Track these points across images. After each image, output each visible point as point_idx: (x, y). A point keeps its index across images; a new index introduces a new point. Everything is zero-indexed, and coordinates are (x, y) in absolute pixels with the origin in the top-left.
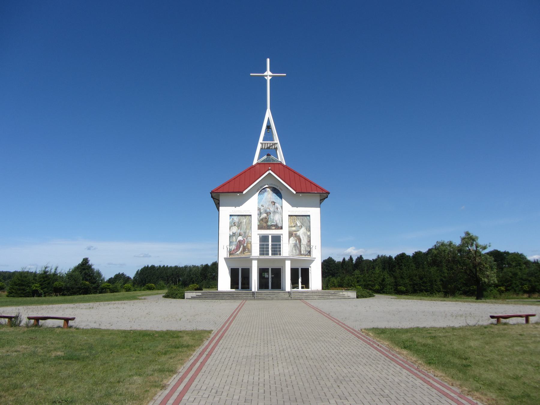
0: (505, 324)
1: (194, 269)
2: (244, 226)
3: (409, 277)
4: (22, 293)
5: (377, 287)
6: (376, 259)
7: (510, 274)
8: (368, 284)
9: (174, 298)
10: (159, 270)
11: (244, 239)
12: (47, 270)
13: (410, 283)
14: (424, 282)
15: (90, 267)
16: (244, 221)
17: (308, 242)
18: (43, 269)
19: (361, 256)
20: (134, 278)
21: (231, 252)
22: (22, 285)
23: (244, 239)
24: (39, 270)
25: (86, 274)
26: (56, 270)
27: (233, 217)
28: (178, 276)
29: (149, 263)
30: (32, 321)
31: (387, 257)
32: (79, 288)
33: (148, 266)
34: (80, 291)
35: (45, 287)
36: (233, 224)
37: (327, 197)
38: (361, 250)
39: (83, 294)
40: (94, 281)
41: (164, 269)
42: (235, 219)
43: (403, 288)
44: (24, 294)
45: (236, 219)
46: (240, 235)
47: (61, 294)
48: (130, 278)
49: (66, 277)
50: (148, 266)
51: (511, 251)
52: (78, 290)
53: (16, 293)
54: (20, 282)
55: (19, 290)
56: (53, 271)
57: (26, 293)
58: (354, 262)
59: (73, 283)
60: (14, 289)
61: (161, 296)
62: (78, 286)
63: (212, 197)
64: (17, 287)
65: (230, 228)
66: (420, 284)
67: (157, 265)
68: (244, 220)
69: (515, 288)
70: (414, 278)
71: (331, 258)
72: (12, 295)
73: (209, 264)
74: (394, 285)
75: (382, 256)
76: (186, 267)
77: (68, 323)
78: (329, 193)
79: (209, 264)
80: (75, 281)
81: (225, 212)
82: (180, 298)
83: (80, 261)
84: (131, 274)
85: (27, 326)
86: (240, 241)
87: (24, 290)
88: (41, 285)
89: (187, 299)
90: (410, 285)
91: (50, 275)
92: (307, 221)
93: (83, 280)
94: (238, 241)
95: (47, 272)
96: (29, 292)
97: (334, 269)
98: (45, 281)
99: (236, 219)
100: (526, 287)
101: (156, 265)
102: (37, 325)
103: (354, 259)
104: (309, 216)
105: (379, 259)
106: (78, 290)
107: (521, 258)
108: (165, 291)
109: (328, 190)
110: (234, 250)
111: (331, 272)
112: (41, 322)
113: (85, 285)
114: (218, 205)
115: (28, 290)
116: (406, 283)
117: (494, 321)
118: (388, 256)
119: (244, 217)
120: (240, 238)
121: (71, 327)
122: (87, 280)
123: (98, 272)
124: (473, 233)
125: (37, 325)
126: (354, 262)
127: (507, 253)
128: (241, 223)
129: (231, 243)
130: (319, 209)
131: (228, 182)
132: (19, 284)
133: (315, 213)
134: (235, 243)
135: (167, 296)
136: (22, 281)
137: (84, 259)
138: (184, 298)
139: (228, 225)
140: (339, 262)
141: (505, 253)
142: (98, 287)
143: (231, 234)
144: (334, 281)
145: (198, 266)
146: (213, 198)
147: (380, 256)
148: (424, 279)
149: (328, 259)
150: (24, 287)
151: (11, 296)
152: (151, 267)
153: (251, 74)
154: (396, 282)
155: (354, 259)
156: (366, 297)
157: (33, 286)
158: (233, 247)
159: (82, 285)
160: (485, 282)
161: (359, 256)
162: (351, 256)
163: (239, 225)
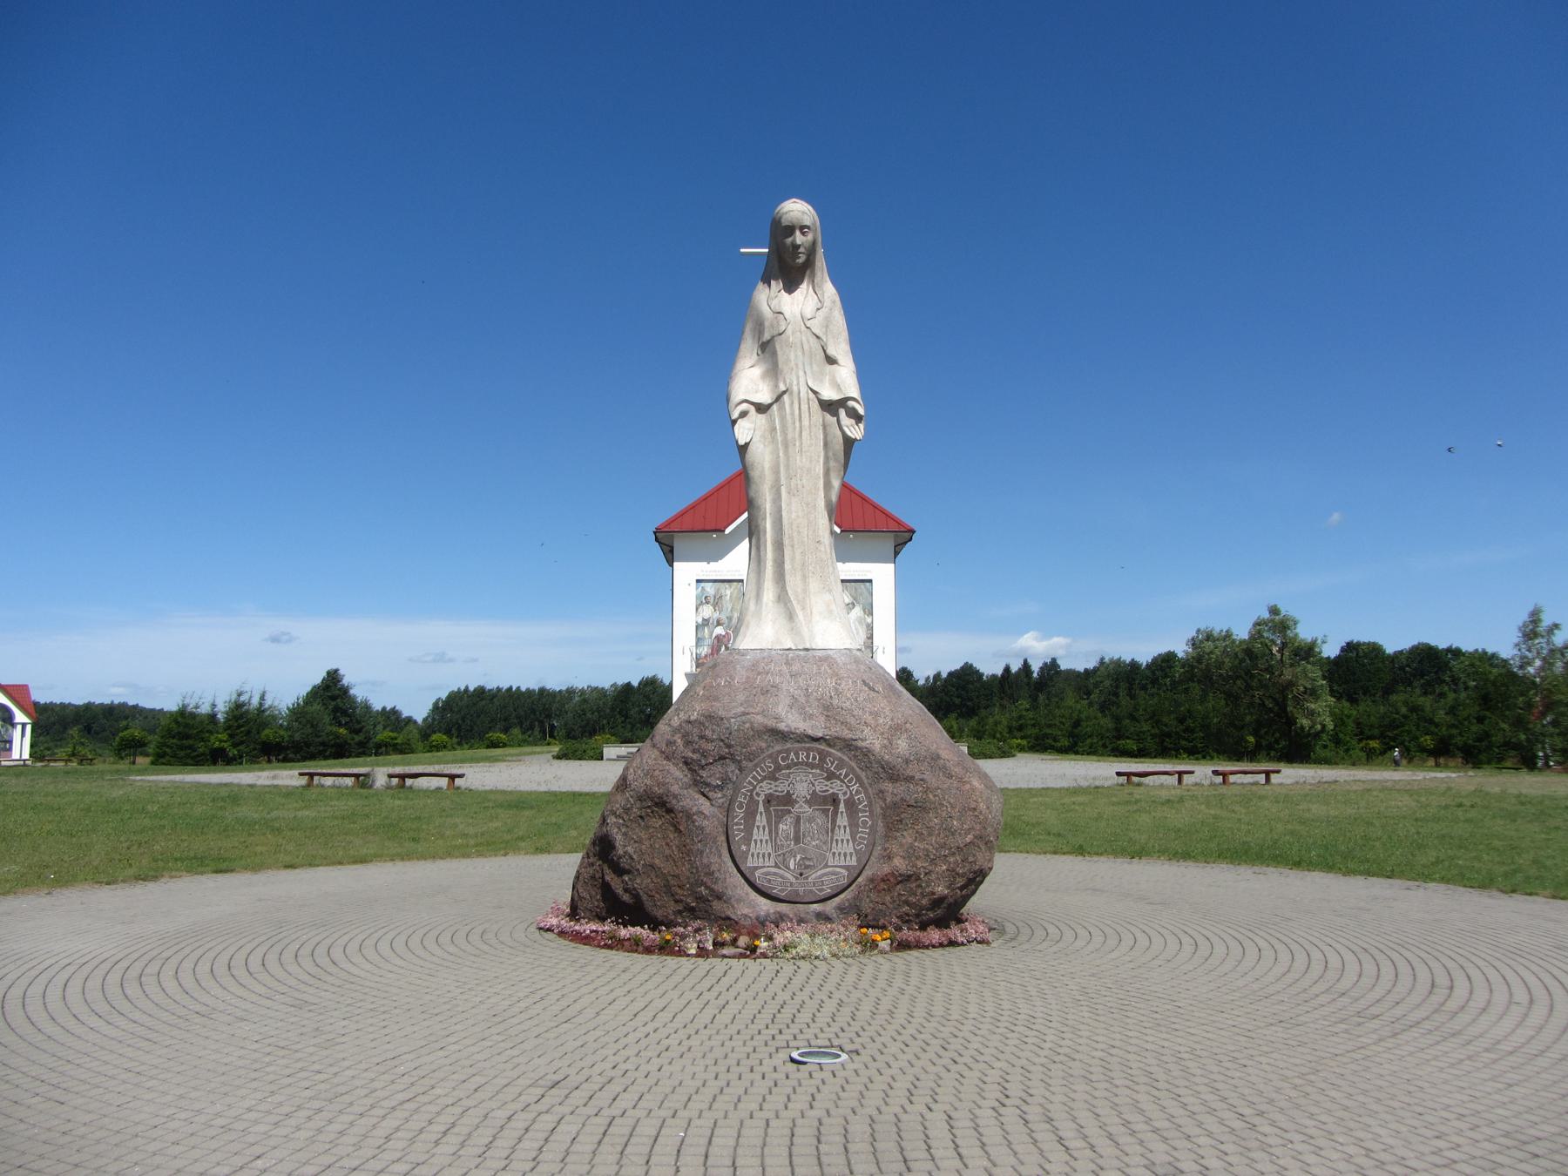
0: (1139, 785)
1: (595, 695)
2: (727, 603)
3: (1151, 718)
4: (187, 756)
5: (1065, 742)
6: (1096, 670)
7: (1404, 710)
8: (1046, 736)
9: (580, 759)
10: (495, 700)
11: (727, 633)
12: (242, 699)
13: (1153, 731)
14: (1187, 730)
15: (345, 691)
16: (728, 592)
17: (868, 638)
18: (234, 697)
19: (1054, 660)
20: (425, 720)
21: (701, 661)
22: (188, 737)
23: (727, 633)
24: (170, 704)
25: (336, 709)
26: (262, 698)
27: (703, 584)
28: (549, 716)
29: (471, 679)
30: (395, 781)
31: (1124, 662)
32: (323, 744)
33: (467, 687)
34: (325, 751)
35: (242, 743)
36: (702, 601)
37: (911, 539)
38: (1056, 640)
39: (334, 758)
40: (358, 727)
41: (512, 698)
42: (708, 589)
43: (1131, 745)
44: (192, 758)
45: (710, 589)
46: (719, 623)
47: (280, 757)
48: (415, 722)
49: (290, 716)
50: (467, 687)
51: (1467, 646)
52: (321, 748)
53: (174, 756)
54: (181, 729)
55: (182, 748)
56: (255, 701)
57: (198, 756)
58: (1035, 675)
59: (310, 731)
60: (168, 746)
61: (549, 756)
62: (320, 739)
63: (657, 540)
64: (175, 741)
65: (697, 609)
66: (1177, 733)
67: (491, 685)
68: (728, 591)
69: (1407, 743)
70: (1165, 719)
71: (971, 665)
72: (164, 761)
73: (635, 683)
74: (1113, 737)
75: (1112, 661)
76: (570, 692)
77: (454, 781)
78: (914, 532)
79: (635, 683)
80: (312, 726)
81: (687, 573)
82: (592, 758)
83: (317, 678)
84: (418, 709)
85: (389, 787)
86: (718, 637)
87: (190, 747)
88: (231, 736)
89: (608, 760)
90: (1153, 736)
91: (247, 711)
92: (866, 593)
93: (331, 725)
94: (714, 636)
95: (243, 704)
96: (203, 754)
97: (978, 697)
98: (239, 727)
99: (710, 589)
100: (1427, 741)
101: (488, 687)
102: (402, 786)
103: (1036, 667)
104: (870, 581)
105: (1102, 669)
106: (321, 748)
107: (1491, 665)
108: (556, 749)
109: (913, 525)
110: (706, 656)
111: (969, 703)
112: (409, 782)
113: (337, 736)
114: (671, 563)
115: (201, 748)
116: (1143, 733)
117: (1123, 779)
118: (1128, 660)
119: (727, 585)
120: (719, 630)
121: (458, 788)
122: (340, 725)
123: (366, 704)
124: (1286, 609)
125: (402, 786)
126: (1035, 675)
127: (1456, 653)
128: (721, 597)
129: (699, 641)
130: (892, 566)
131: (693, 507)
132: (179, 733)
133: (882, 575)
134: (708, 642)
135: (558, 757)
136: (187, 725)
137: (328, 673)
138: (602, 759)
139: (693, 603)
140: (994, 676)
141: (1449, 650)
142: (368, 742)
143: (700, 621)
144: (952, 727)
145: (603, 688)
146: (660, 543)
147: (1107, 660)
148: (1189, 722)
149: (962, 668)
150: (191, 742)
151: (163, 764)
152: (475, 690)
153: (742, 250)
154: (1117, 730)
155: (1036, 667)
156: (991, 757)
157: (212, 738)
158: (705, 650)
159: (331, 737)
160: (1302, 728)
161: (1048, 661)
162: (1026, 662)
163: (717, 602)
